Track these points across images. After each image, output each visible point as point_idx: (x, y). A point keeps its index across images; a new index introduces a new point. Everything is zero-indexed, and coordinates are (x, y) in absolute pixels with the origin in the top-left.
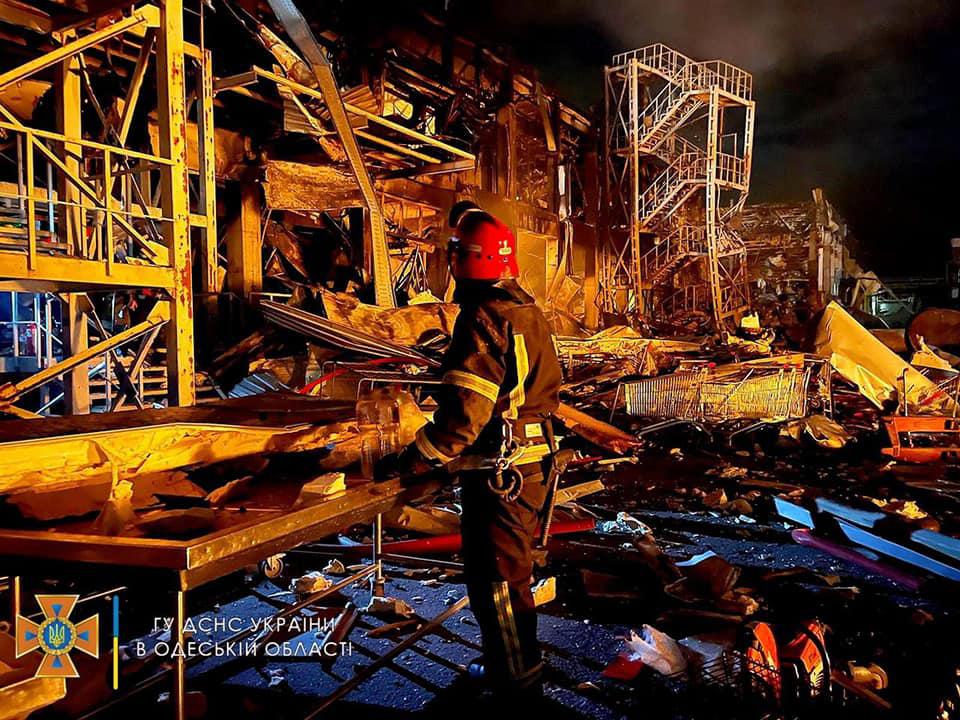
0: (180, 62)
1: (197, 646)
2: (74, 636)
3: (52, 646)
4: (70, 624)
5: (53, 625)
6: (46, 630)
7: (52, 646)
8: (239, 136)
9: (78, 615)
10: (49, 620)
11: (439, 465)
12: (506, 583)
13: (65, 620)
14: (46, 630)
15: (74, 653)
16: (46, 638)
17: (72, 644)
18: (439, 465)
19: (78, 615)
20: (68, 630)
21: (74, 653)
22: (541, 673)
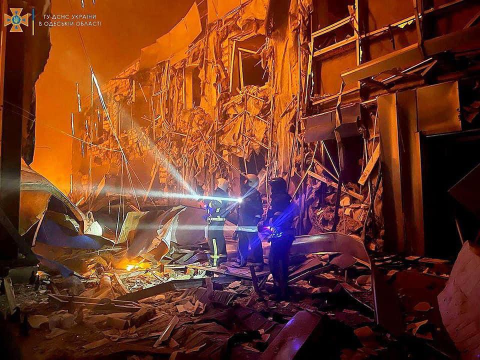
0: (56, 292)
1: (56, 23)
2: (21, 20)
3: (15, 23)
4: (20, 17)
5: (15, 17)
6: (13, 18)
7: (15, 23)
8: (10, 314)
9: (10, 14)
10: (14, 15)
11: (312, 75)
12: (22, 322)
13: (19, 16)
14: (13, 18)
15: (21, 25)
16: (13, 21)
17: (20, 22)
18: (312, 75)
19: (10, 14)
20: (19, 18)
21: (21, 25)
22: (371, 95)
